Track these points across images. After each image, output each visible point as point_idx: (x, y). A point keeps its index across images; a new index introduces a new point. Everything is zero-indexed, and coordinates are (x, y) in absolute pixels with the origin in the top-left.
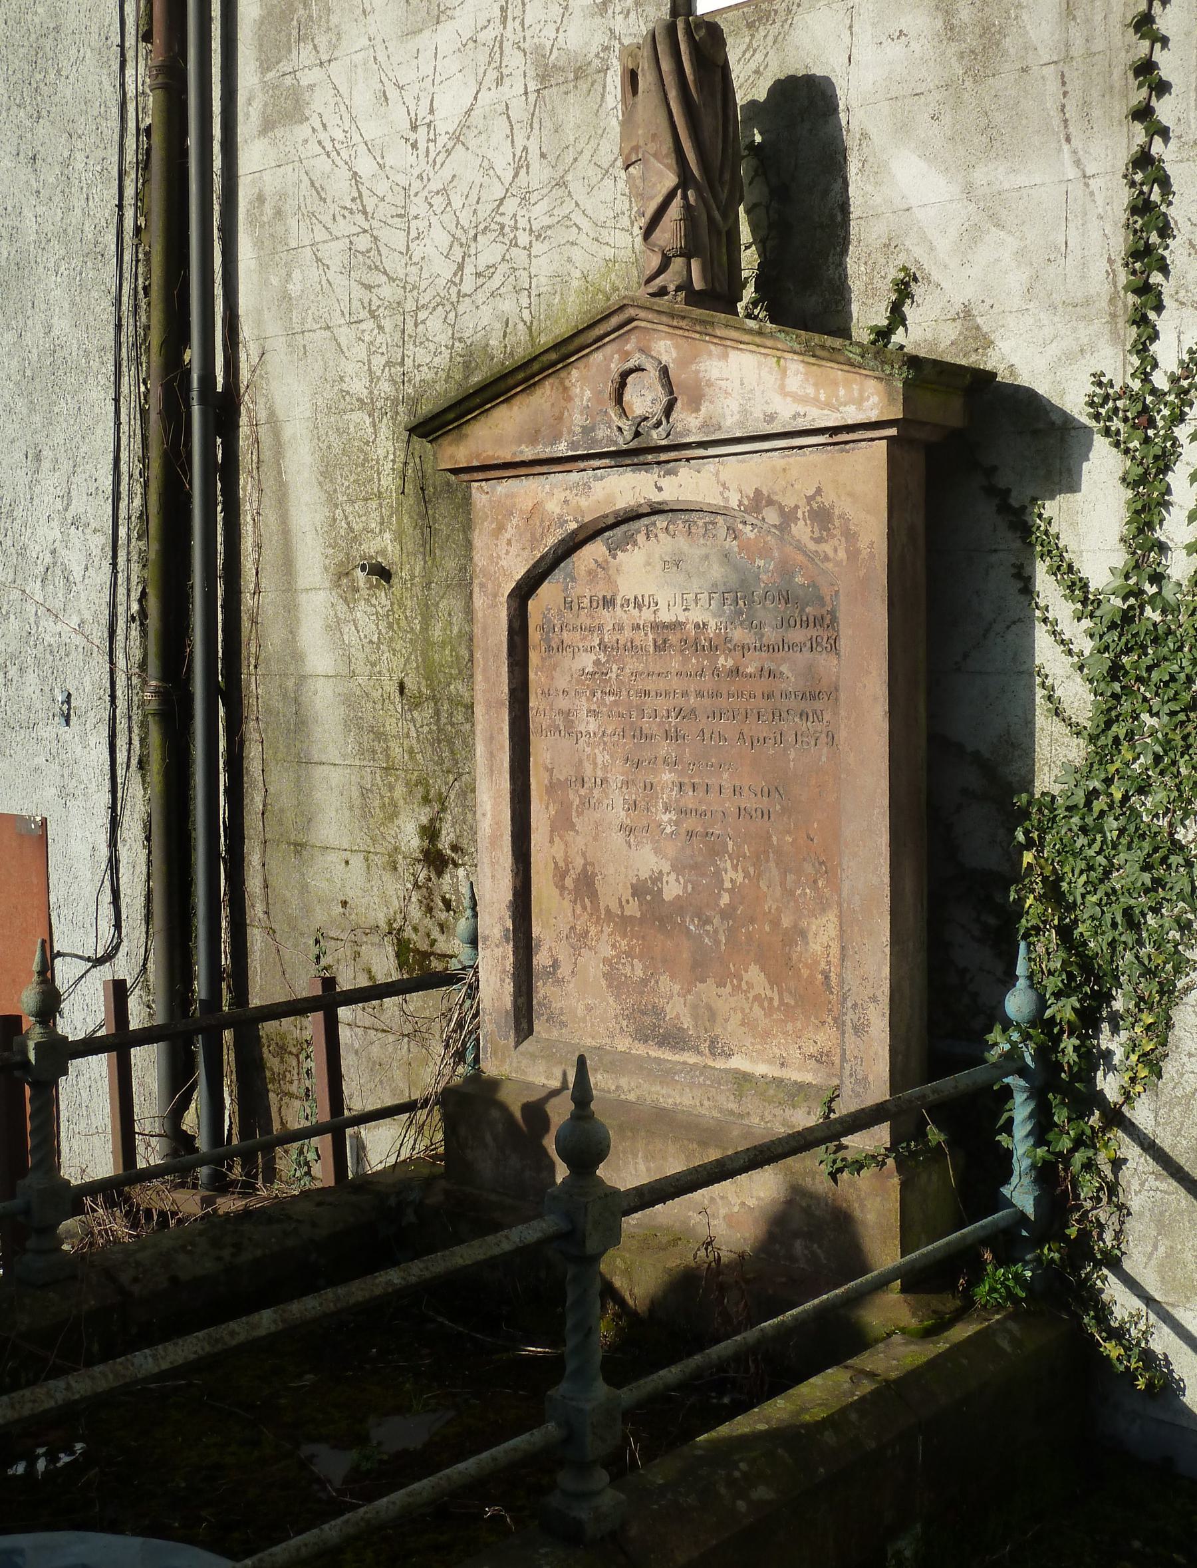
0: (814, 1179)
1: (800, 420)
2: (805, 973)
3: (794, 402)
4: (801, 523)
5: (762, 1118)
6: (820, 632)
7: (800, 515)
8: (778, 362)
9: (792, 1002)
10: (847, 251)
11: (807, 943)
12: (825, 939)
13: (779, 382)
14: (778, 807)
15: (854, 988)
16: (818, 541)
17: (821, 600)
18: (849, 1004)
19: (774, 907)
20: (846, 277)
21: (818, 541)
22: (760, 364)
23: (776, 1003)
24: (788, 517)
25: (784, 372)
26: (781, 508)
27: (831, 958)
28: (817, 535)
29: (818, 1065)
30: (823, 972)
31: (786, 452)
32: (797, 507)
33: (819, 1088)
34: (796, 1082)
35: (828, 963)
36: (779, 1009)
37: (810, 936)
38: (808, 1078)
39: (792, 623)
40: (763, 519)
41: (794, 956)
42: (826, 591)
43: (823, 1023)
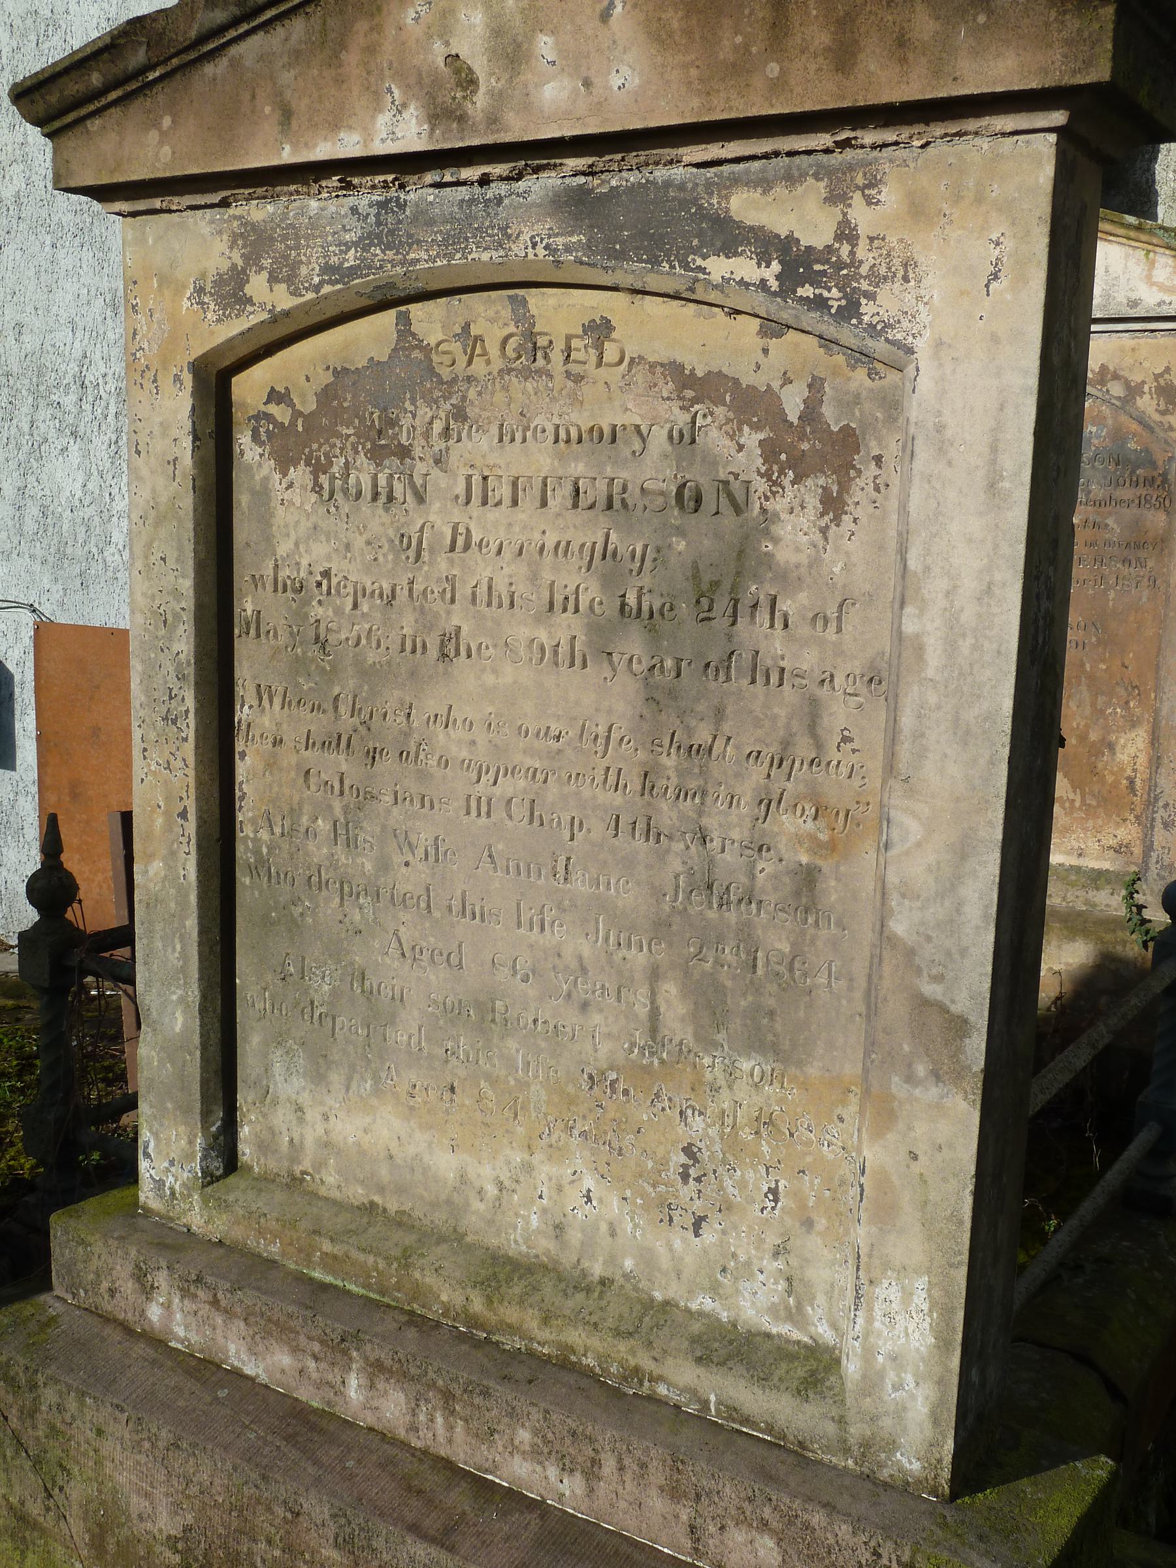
0: (1124, 946)
1: (1165, 307)
2: (1110, 779)
3: (1160, 291)
4: (1147, 397)
5: (1064, 899)
6: (1150, 491)
7: (1146, 388)
8: (1147, 255)
9: (1094, 803)
10: (1156, 158)
11: (1114, 754)
12: (1132, 751)
13: (1145, 273)
14: (1094, 639)
15: (1167, 791)
16: (1163, 413)
17: (1153, 464)
18: (1161, 804)
19: (1082, 724)
20: (1154, 181)
21: (1163, 413)
22: (1127, 256)
23: (1077, 804)
24: (1133, 391)
25: (1152, 264)
26: (1127, 384)
27: (1138, 766)
28: (1162, 407)
29: (1117, 855)
30: (1128, 778)
31: (1137, 334)
32: (1144, 382)
33: (1117, 875)
34: (1093, 869)
35: (1135, 770)
36: (1080, 809)
37: (1118, 748)
38: (1106, 865)
39: (1121, 481)
40: (1108, 391)
41: (1100, 765)
42: (1160, 458)
43: (1125, 820)
